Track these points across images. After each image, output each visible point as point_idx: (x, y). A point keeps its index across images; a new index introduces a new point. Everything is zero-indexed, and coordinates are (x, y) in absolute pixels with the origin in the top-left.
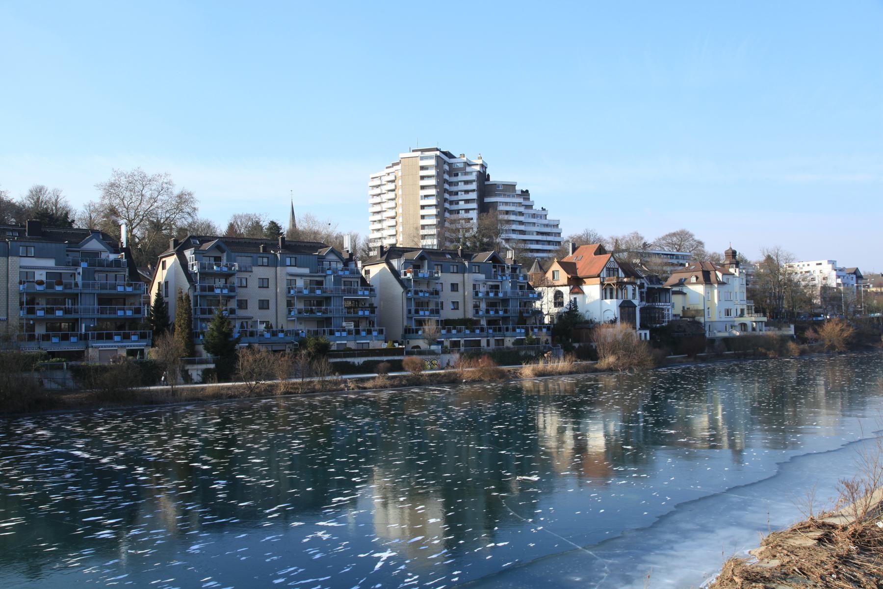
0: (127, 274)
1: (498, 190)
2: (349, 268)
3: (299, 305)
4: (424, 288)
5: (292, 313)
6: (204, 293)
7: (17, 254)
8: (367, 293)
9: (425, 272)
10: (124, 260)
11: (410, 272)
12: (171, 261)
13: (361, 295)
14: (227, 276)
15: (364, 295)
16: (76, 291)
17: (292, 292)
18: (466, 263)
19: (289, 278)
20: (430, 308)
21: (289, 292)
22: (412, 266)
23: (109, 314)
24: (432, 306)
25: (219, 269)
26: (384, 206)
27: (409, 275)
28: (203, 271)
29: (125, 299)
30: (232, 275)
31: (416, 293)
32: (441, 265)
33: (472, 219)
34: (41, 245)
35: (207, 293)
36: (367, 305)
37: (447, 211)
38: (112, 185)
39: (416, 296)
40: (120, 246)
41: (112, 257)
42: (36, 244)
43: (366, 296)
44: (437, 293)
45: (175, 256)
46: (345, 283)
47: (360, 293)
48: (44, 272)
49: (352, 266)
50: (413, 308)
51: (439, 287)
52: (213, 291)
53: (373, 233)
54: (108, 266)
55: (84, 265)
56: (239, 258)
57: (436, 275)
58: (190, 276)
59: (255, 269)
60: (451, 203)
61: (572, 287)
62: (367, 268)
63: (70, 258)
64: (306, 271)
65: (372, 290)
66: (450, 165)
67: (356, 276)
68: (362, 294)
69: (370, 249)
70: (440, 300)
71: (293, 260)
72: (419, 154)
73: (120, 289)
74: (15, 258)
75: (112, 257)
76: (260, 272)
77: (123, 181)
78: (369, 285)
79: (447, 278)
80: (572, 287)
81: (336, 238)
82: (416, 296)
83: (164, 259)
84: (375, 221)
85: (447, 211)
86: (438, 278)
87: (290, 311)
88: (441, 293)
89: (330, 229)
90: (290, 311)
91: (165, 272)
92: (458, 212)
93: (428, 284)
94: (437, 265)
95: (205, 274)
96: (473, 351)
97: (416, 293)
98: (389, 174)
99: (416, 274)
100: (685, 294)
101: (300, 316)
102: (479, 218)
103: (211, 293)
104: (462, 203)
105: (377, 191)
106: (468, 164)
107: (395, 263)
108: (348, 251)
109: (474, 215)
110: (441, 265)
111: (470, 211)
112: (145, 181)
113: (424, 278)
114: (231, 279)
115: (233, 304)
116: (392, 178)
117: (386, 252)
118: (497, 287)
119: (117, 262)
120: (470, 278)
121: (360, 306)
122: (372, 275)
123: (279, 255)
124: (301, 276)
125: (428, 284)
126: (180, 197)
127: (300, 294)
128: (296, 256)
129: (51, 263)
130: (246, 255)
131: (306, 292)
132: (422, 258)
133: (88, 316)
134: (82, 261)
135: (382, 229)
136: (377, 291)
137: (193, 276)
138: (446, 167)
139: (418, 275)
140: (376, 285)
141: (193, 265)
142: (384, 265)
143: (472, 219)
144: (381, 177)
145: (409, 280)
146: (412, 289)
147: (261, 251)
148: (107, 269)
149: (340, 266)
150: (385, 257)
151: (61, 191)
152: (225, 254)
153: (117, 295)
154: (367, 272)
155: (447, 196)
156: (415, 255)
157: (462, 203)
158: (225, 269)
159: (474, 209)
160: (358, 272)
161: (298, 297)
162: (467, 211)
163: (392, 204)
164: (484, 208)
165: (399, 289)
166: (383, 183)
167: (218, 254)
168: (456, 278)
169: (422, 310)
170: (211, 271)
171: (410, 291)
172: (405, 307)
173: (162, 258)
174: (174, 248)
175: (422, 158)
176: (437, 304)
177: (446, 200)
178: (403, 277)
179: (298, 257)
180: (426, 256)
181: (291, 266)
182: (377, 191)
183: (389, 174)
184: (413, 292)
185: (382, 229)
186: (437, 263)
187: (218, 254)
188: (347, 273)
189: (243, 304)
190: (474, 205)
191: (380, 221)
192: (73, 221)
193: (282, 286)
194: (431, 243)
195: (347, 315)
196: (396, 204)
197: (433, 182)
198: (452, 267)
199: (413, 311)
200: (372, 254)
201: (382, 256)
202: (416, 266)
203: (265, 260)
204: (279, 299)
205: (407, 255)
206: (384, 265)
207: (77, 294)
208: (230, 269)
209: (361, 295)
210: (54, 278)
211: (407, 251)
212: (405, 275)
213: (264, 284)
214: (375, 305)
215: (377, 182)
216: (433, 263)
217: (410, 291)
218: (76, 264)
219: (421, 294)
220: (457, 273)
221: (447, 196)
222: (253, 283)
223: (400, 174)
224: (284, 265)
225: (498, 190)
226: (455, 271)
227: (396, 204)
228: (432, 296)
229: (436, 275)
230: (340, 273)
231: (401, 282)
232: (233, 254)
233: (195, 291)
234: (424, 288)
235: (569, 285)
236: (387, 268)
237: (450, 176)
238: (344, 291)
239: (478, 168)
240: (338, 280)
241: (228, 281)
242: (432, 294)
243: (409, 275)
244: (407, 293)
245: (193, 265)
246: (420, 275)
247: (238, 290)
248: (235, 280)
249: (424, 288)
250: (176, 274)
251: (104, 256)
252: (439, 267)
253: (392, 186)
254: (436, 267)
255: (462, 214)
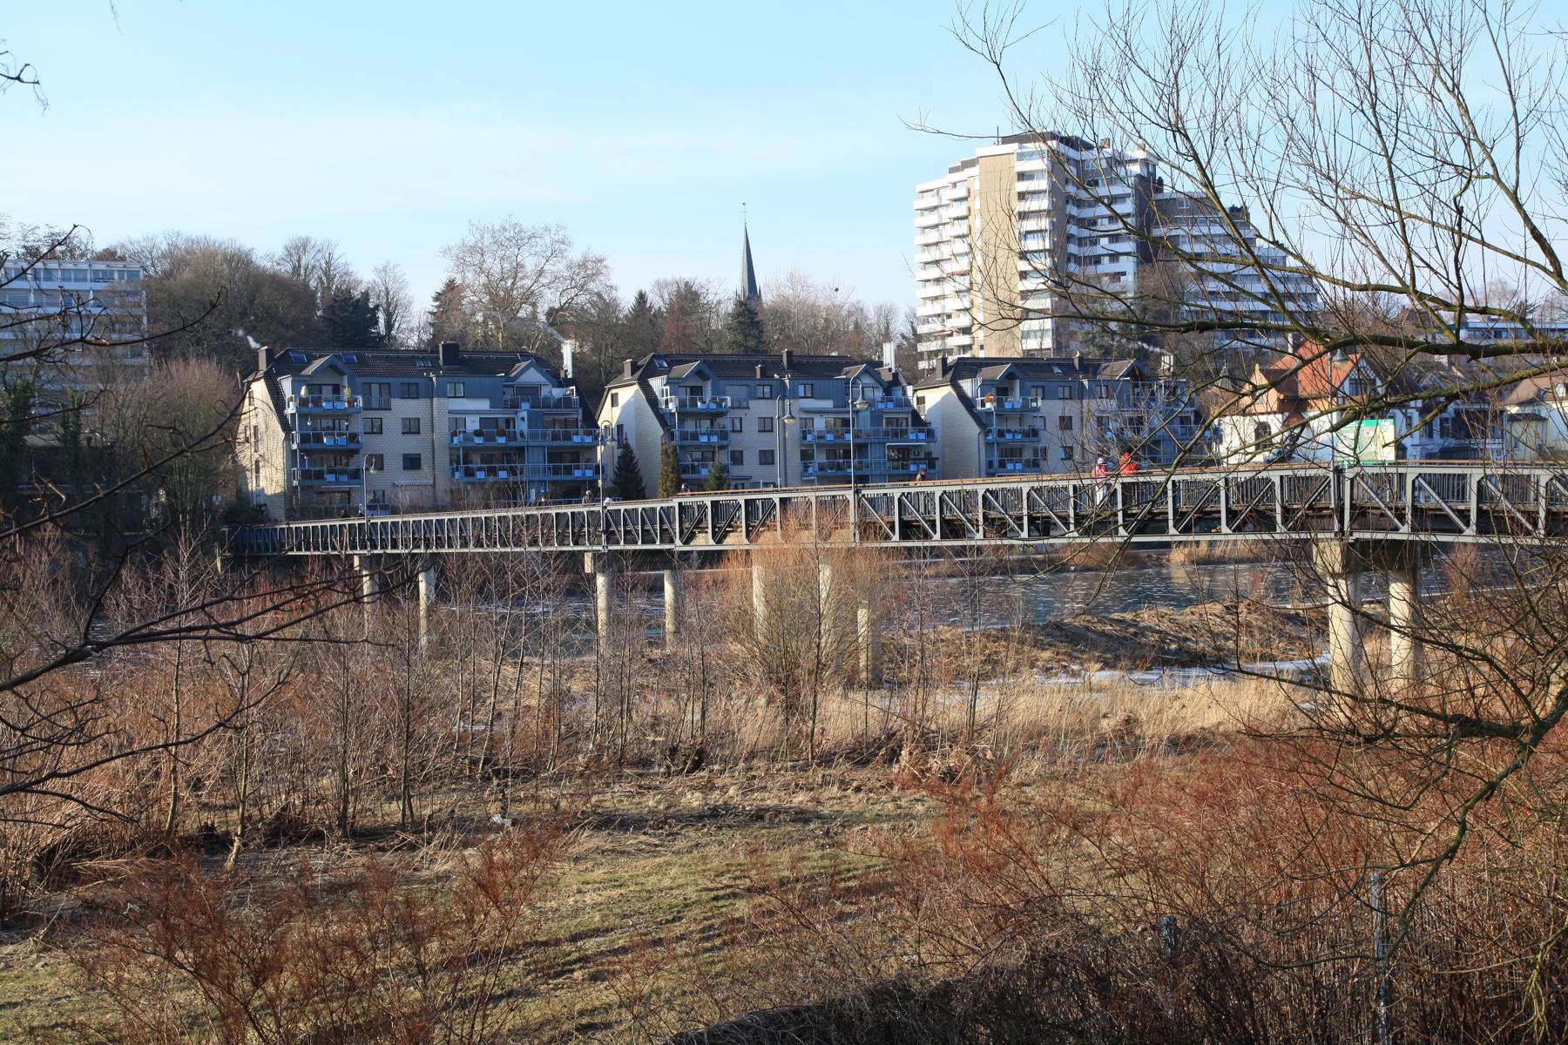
0: (580, 418)
1: (1181, 212)
2: (894, 397)
3: (820, 458)
4: (1014, 425)
5: (810, 470)
6: (685, 443)
7: (444, 395)
8: (922, 436)
9: (1015, 400)
10: (575, 397)
11: (991, 401)
12: (628, 394)
13: (912, 441)
14: (713, 416)
15: (917, 440)
16: (522, 444)
17: (809, 437)
18: (1086, 382)
19: (803, 416)
20: (1024, 458)
21: (805, 438)
22: (994, 390)
23: (1066, 489)
24: (1028, 455)
25: (704, 407)
26: (946, 251)
27: (988, 405)
28: (683, 410)
29: (578, 454)
30: (722, 415)
31: (1001, 434)
32: (1043, 387)
33: (1124, 274)
34: (472, 380)
35: (689, 442)
36: (922, 456)
37: (1073, 259)
38: (473, 250)
39: (1001, 440)
40: (562, 375)
41: (557, 393)
42: (467, 380)
43: (922, 441)
44: (1034, 433)
45: (636, 387)
46: (889, 421)
47: (912, 437)
48: (477, 418)
49: (897, 393)
50: (996, 459)
51: (1038, 424)
52: (697, 439)
53: (925, 304)
54: (555, 407)
55: (525, 406)
56: (729, 389)
57: (1034, 404)
58: (662, 417)
59: (753, 404)
60: (1081, 242)
61: (1287, 414)
62: (920, 394)
63: (508, 397)
64: (828, 404)
65: (930, 434)
66: (1078, 164)
67: (907, 409)
68: (914, 438)
69: (919, 338)
70: (1041, 445)
71: (809, 388)
72: (1014, 147)
73: (576, 439)
74: (442, 400)
75: (557, 393)
76: (759, 408)
77: (487, 240)
78: (925, 424)
79: (1051, 409)
80: (1287, 414)
81: (850, 314)
82: (1001, 440)
83: (613, 391)
84: (929, 281)
85: (1073, 259)
86: (1037, 409)
87: (806, 467)
88: (1042, 434)
89: (839, 298)
90: (806, 467)
91: (617, 411)
92: (1097, 260)
93: (1021, 419)
94: (1037, 387)
95: (684, 415)
96: (1203, 548)
97: (1001, 434)
98: (954, 185)
99: (1000, 403)
100: (1544, 420)
101: (823, 473)
102: (1139, 275)
103: (694, 442)
104: (1104, 241)
105: (932, 219)
106: (1118, 161)
107: (967, 386)
108: (890, 370)
109: (1127, 265)
110: (1043, 387)
111: (1121, 258)
112: (521, 239)
113: (1013, 410)
114: (720, 421)
115: (723, 458)
116: (960, 192)
117: (951, 367)
118: (1140, 421)
119: (566, 401)
120: (1091, 405)
121: (912, 456)
122: (929, 404)
123: (787, 382)
124: (821, 412)
125: (1021, 419)
126: (583, 265)
127: (821, 441)
128: (814, 382)
129: (484, 405)
130: (740, 382)
131: (830, 437)
132: (1010, 376)
133: (537, 478)
134: (523, 400)
135: (944, 297)
136: (938, 434)
137: (667, 418)
138: (1073, 170)
139: (1003, 406)
140: (936, 425)
141: (667, 401)
142: (947, 390)
143: (1124, 274)
144: (938, 189)
145: (989, 413)
146: (994, 428)
147: (758, 376)
148: (555, 411)
149: (879, 394)
150: (949, 375)
151: (336, 246)
152: (709, 383)
153: (572, 447)
154: (921, 401)
155: (1073, 229)
156: (1002, 370)
157: (1104, 241)
158: (713, 406)
159: (1128, 254)
160: (908, 403)
161: (819, 446)
162: (1114, 257)
163: (961, 247)
164: (1148, 252)
165: (974, 429)
166: (944, 203)
167: (696, 382)
168: (1071, 408)
169: (1011, 461)
170: (694, 410)
171: (990, 431)
172: (983, 457)
173: (610, 389)
174: (633, 373)
175: (1021, 157)
176: (1036, 451)
177: (1070, 238)
178: (979, 408)
179: (816, 383)
180: (1017, 373)
181: (805, 397)
182: (932, 219)
183: (954, 185)
184: (995, 433)
185: (944, 297)
186: (1036, 384)
187: (696, 382)
188: (891, 405)
189: (737, 458)
190: (1128, 246)
191: (938, 280)
192: (366, 296)
193: (442, 427)
194: (1037, 338)
195: (892, 472)
196: (969, 209)
197: (1044, 203)
198: (1061, 389)
199: (996, 464)
200: (923, 365)
201: (945, 372)
202: (1002, 391)
203: (767, 389)
204: (788, 448)
205: (987, 372)
206: (948, 390)
207: (523, 448)
208: (719, 405)
209: (912, 441)
210: (489, 426)
211: (987, 365)
212: (983, 405)
213: (766, 426)
214: (934, 455)
215: (931, 201)
216: (1028, 384)
217: (990, 431)
218: (515, 405)
219: (1009, 436)
220: (1071, 398)
221: (1073, 229)
222: (751, 425)
223: (976, 186)
224: (795, 396)
225: (1181, 212)
226: (1067, 395)
227: (969, 209)
228: (1027, 439)
229: (1034, 404)
230: (881, 406)
231: (977, 417)
232: (721, 382)
233: (672, 439)
234: (1014, 425)
235: (1281, 411)
236: (954, 394)
237: (1079, 186)
238: (886, 433)
239: (1136, 169)
240: (876, 417)
241: (715, 423)
242: (1026, 434)
243: (988, 405)
244: (987, 435)
245: (667, 401)
246: (1007, 405)
247: (733, 436)
248: (725, 422)
249: (1014, 425)
250: (638, 413)
251: (545, 392)
252: (1040, 391)
253: (961, 210)
254: (1034, 390)
255: (1107, 266)
